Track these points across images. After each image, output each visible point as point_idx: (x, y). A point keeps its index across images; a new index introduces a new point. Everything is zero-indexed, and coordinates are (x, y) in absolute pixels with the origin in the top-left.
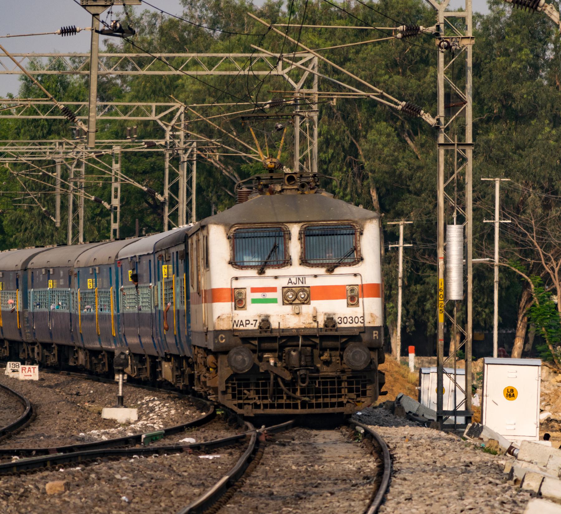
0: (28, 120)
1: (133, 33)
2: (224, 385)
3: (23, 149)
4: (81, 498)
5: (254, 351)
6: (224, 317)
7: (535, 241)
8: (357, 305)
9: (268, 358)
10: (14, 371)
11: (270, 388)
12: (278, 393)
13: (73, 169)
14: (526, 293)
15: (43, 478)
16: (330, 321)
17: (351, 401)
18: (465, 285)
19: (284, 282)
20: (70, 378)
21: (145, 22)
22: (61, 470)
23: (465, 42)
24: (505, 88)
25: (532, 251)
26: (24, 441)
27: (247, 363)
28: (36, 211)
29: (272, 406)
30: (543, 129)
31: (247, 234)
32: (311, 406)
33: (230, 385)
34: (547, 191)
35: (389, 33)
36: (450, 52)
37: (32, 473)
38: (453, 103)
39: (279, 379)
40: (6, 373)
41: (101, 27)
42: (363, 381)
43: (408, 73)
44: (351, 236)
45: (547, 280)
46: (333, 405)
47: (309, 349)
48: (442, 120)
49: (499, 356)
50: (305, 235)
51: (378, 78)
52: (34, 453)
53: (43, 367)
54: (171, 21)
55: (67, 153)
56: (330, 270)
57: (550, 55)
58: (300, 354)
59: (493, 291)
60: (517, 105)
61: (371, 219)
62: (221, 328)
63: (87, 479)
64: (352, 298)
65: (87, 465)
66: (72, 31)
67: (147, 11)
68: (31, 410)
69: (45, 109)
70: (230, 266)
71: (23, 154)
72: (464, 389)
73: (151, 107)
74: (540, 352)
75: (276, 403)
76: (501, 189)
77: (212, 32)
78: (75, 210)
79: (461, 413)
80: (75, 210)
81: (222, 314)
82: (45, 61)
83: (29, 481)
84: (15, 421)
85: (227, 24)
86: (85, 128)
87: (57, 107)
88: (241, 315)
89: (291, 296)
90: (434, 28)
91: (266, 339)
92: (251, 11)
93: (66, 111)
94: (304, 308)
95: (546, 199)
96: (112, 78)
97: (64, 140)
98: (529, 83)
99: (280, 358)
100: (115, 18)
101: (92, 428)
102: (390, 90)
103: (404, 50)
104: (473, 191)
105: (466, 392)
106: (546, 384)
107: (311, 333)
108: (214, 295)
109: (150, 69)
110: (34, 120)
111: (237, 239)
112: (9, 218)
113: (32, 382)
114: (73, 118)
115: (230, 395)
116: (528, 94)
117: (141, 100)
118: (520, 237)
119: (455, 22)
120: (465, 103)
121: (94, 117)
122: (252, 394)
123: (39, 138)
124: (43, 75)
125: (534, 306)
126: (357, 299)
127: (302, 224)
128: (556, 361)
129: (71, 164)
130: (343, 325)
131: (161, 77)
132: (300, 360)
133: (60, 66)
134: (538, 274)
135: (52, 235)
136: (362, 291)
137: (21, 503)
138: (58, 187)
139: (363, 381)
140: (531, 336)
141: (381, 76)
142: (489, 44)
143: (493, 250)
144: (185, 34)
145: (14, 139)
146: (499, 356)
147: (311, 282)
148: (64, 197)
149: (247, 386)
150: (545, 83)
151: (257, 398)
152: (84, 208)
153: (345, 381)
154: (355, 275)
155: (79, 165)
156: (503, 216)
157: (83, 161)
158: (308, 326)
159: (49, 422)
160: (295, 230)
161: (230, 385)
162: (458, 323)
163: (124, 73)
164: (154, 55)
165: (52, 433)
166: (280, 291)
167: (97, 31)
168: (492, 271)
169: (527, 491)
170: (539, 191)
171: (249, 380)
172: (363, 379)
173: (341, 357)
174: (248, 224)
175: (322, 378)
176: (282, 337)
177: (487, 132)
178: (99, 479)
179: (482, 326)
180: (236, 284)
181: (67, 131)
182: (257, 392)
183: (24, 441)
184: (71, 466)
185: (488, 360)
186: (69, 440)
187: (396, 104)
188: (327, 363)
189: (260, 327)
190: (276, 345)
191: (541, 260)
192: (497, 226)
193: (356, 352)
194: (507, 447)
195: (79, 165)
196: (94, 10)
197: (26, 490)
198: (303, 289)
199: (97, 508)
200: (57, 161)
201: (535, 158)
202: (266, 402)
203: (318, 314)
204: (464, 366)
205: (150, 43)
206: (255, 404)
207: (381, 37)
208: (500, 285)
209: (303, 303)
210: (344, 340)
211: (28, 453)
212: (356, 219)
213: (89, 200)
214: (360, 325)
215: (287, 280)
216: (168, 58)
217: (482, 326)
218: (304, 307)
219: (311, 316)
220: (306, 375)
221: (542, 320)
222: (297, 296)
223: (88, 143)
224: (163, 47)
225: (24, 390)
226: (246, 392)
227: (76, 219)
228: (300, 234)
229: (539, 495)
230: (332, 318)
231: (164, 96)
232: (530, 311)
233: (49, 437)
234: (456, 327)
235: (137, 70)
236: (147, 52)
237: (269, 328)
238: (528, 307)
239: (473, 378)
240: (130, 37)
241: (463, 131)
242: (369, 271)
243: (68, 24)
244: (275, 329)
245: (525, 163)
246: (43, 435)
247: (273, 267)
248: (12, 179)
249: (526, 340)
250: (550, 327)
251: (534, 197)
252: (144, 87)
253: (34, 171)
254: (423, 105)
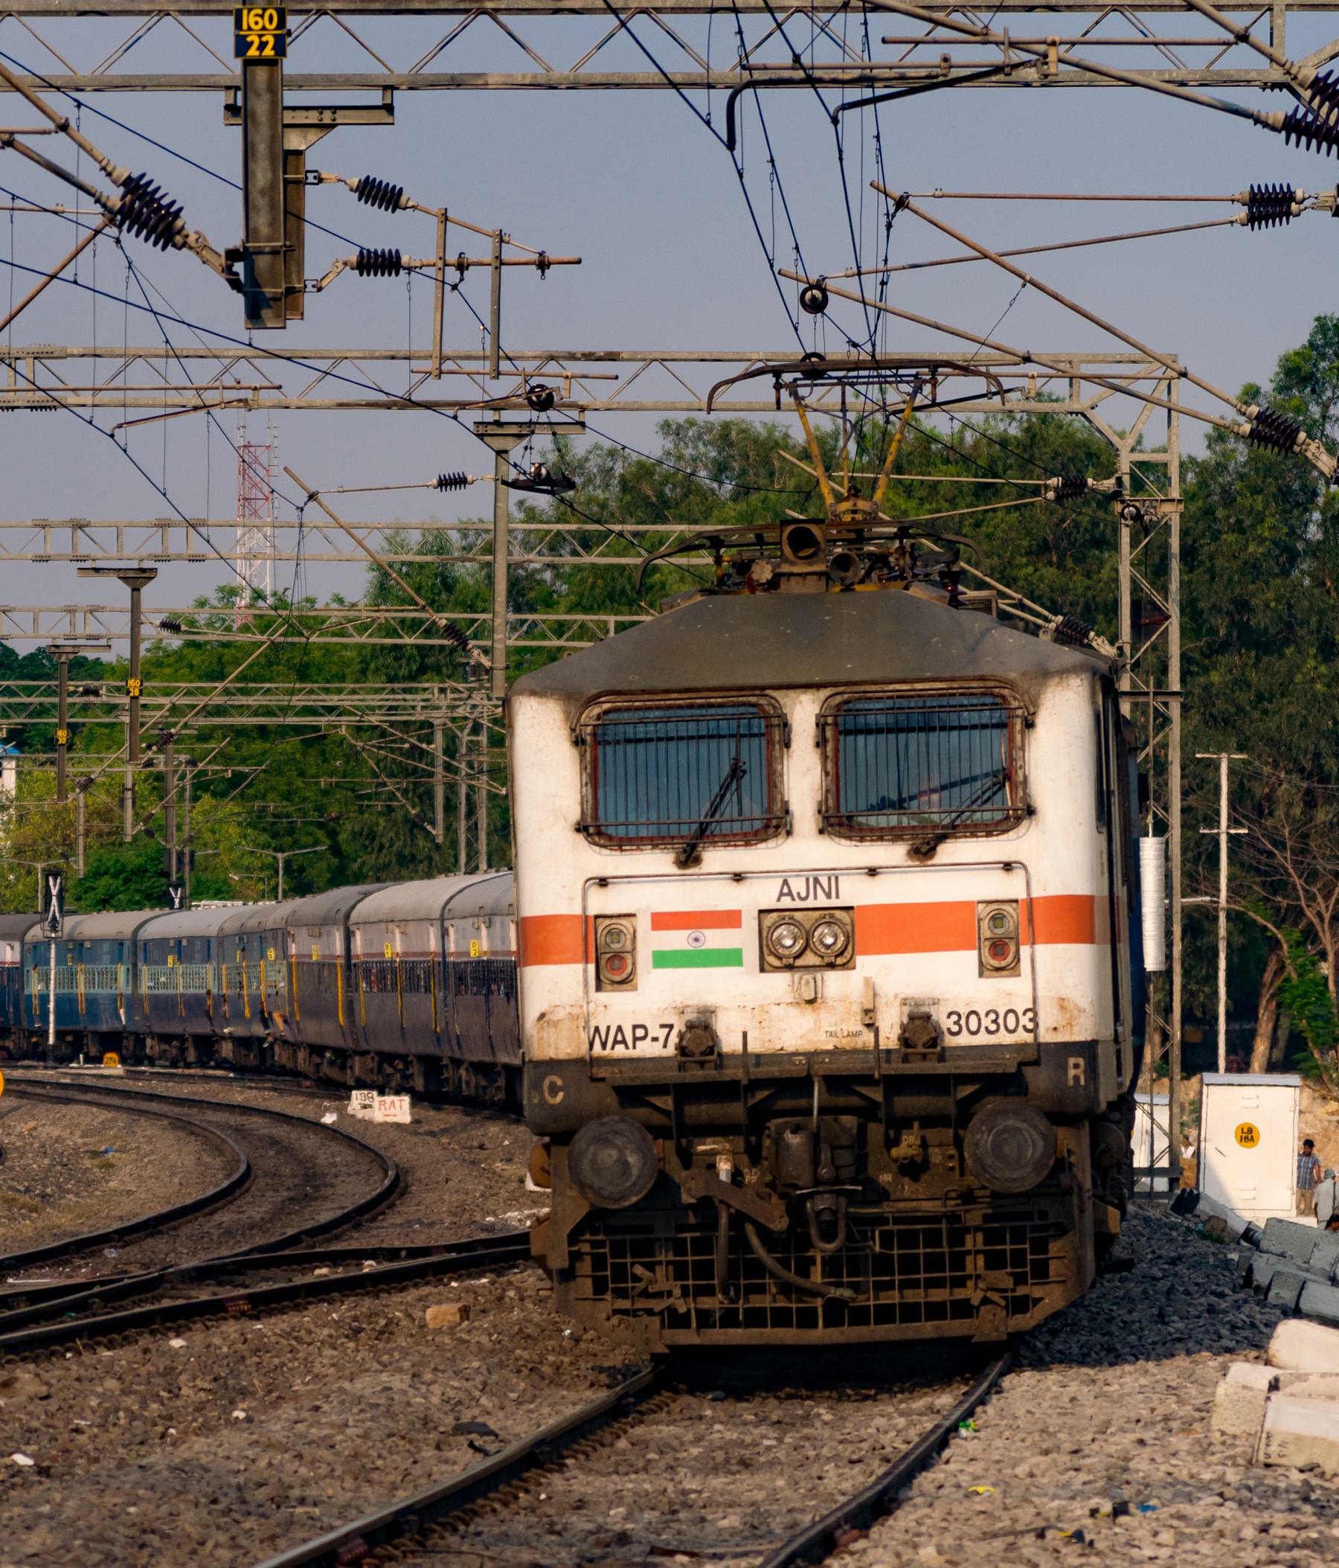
0: (383, 647)
1: (571, 485)
2: (564, 1248)
3: (373, 700)
4: (490, 1335)
5: (658, 1132)
6: (560, 1014)
7: (1289, 866)
8: (1012, 969)
9: (713, 1153)
10: (365, 1107)
11: (719, 1257)
12: (745, 1271)
13: (465, 737)
14: (1274, 959)
15: (420, 1299)
16: (921, 1029)
17: (995, 1297)
18: (1169, 945)
19: (764, 894)
20: (468, 1119)
21: (592, 466)
22: (454, 1284)
23: (1167, 508)
24: (1237, 591)
25: (1286, 883)
26: (387, 1233)
27: (635, 1172)
28: (399, 815)
29: (729, 1319)
30: (1304, 662)
31: (641, 728)
32: (860, 1317)
33: (586, 1248)
34: (1310, 776)
35: (1036, 491)
36: (1141, 526)
37: (401, 1290)
38: (1147, 618)
39: (749, 1229)
40: (350, 1110)
41: (512, 475)
42: (1034, 1229)
43: (1069, 563)
44: (996, 732)
45: (1310, 935)
46: (936, 1311)
47: (850, 1121)
48: (1127, 649)
49: (1228, 1070)
50: (838, 730)
51: (1015, 573)
52: (403, 1253)
53: (417, 1099)
54: (641, 465)
55: (454, 708)
56: (923, 851)
57: (1314, 533)
58: (816, 1139)
59: (1216, 955)
60: (1259, 620)
61: (1063, 672)
62: (551, 1053)
63: (500, 1298)
64: (998, 947)
65: (500, 1273)
66: (459, 481)
67: (598, 447)
68: (397, 1177)
69: (414, 626)
70: (580, 838)
71: (372, 709)
72: (1166, 1128)
73: (605, 623)
74: (1298, 1062)
75: (741, 1305)
76: (1231, 772)
77: (715, 485)
78: (471, 812)
79: (1162, 1172)
80: (471, 812)
82: (415, 538)
83: (395, 1304)
84: (369, 1197)
85: (743, 472)
86: (486, 662)
87: (434, 623)
88: (618, 1009)
89: (788, 942)
90: (1112, 481)
91: (703, 1088)
92: (785, 448)
93: (451, 630)
94: (834, 982)
95: (1309, 792)
96: (536, 571)
97: (450, 684)
98: (1278, 581)
99: (754, 1155)
100: (538, 460)
101: (509, 1208)
102: (1037, 593)
103: (1063, 521)
104: (1183, 777)
105: (1170, 1135)
106: (1308, 1117)
107: (856, 1067)
109: (602, 555)
110: (396, 647)
112: (349, 827)
113: (398, 1126)
114: (463, 642)
115: (589, 1282)
116: (1278, 600)
117: (587, 610)
118: (1264, 859)
119: (1148, 472)
120: (1168, 617)
121: (504, 640)
122: (662, 1279)
123: (405, 679)
124: (411, 564)
125: (1287, 980)
126: (1013, 949)
127: (827, 692)
128: (1325, 1078)
129: (462, 729)
130: (964, 1040)
131: (622, 568)
132: (816, 1162)
133: (441, 547)
134: (1296, 924)
135: (430, 859)
136: (1031, 921)
137: (381, 1345)
138: (439, 770)
139: (1034, 1229)
140: (1283, 1035)
141: (1020, 567)
142: (1209, 512)
143: (1218, 882)
144: (667, 491)
145: (357, 681)
146: (1228, 1070)
147: (856, 892)
148: (451, 788)
149: (644, 1250)
150: (1307, 582)
151: (677, 1292)
152: (488, 809)
153: (977, 1229)
154: (1008, 867)
155: (476, 729)
156: (1234, 822)
157: (485, 722)
158: (846, 1044)
159: (430, 1197)
160: (803, 712)
161: (586, 1248)
162: (1157, 1011)
163: (557, 560)
164: (612, 527)
165: (435, 1218)
166: (750, 923)
167: (504, 483)
168: (1216, 918)
169: (1275, 1306)
170: (1295, 778)
171: (650, 1229)
172: (1037, 1222)
173: (958, 1142)
174: (643, 692)
175: (897, 1221)
176: (756, 1084)
177: (1206, 670)
178: (522, 1299)
179: (1198, 1017)
180: (601, 902)
181: (455, 667)
182: (680, 1272)
183: (387, 1233)
184: (471, 1277)
185: (1208, 1077)
186: (467, 1231)
187: (1047, 620)
188: (913, 1169)
189: (682, 1049)
190: (736, 1111)
191: (1298, 899)
192: (1223, 839)
193: (1006, 1130)
194: (1241, 1229)
195: (476, 729)
196: (499, 443)
197: (390, 1321)
198: (828, 915)
199: (518, 1352)
200: (436, 722)
201: (1289, 717)
202: (706, 1303)
203: (881, 1001)
204: (1167, 1090)
205: (603, 506)
206: (672, 1310)
207: (1022, 497)
208: (1229, 946)
209: (832, 966)
210: (968, 1090)
211: (392, 1254)
212: (1013, 676)
213: (496, 795)
214: (1022, 1037)
215: (776, 885)
216: (636, 534)
217: (1198, 1017)
218: (831, 976)
219: (856, 1009)
220: (835, 1213)
221: (1303, 1006)
222: (808, 941)
223: (491, 688)
224: (627, 513)
225: (384, 1143)
226: (639, 1270)
227: (473, 829)
228: (821, 726)
229: (1297, 1313)
230: (927, 1017)
231: (630, 604)
232: (1281, 989)
233: (432, 1224)
234: (1154, 1019)
235: (578, 555)
236: (598, 522)
237: (711, 1050)
238: (1278, 983)
239: (1182, 1110)
240: (570, 494)
241: (1164, 670)
242: (1056, 847)
243: (450, 470)
244: (732, 1056)
245: (1273, 725)
246: (419, 1221)
247: (729, 840)
248: (353, 756)
249: (1274, 1042)
250: (1315, 1017)
251: (1288, 787)
252: (592, 588)
253: (395, 741)
254: (1093, 622)
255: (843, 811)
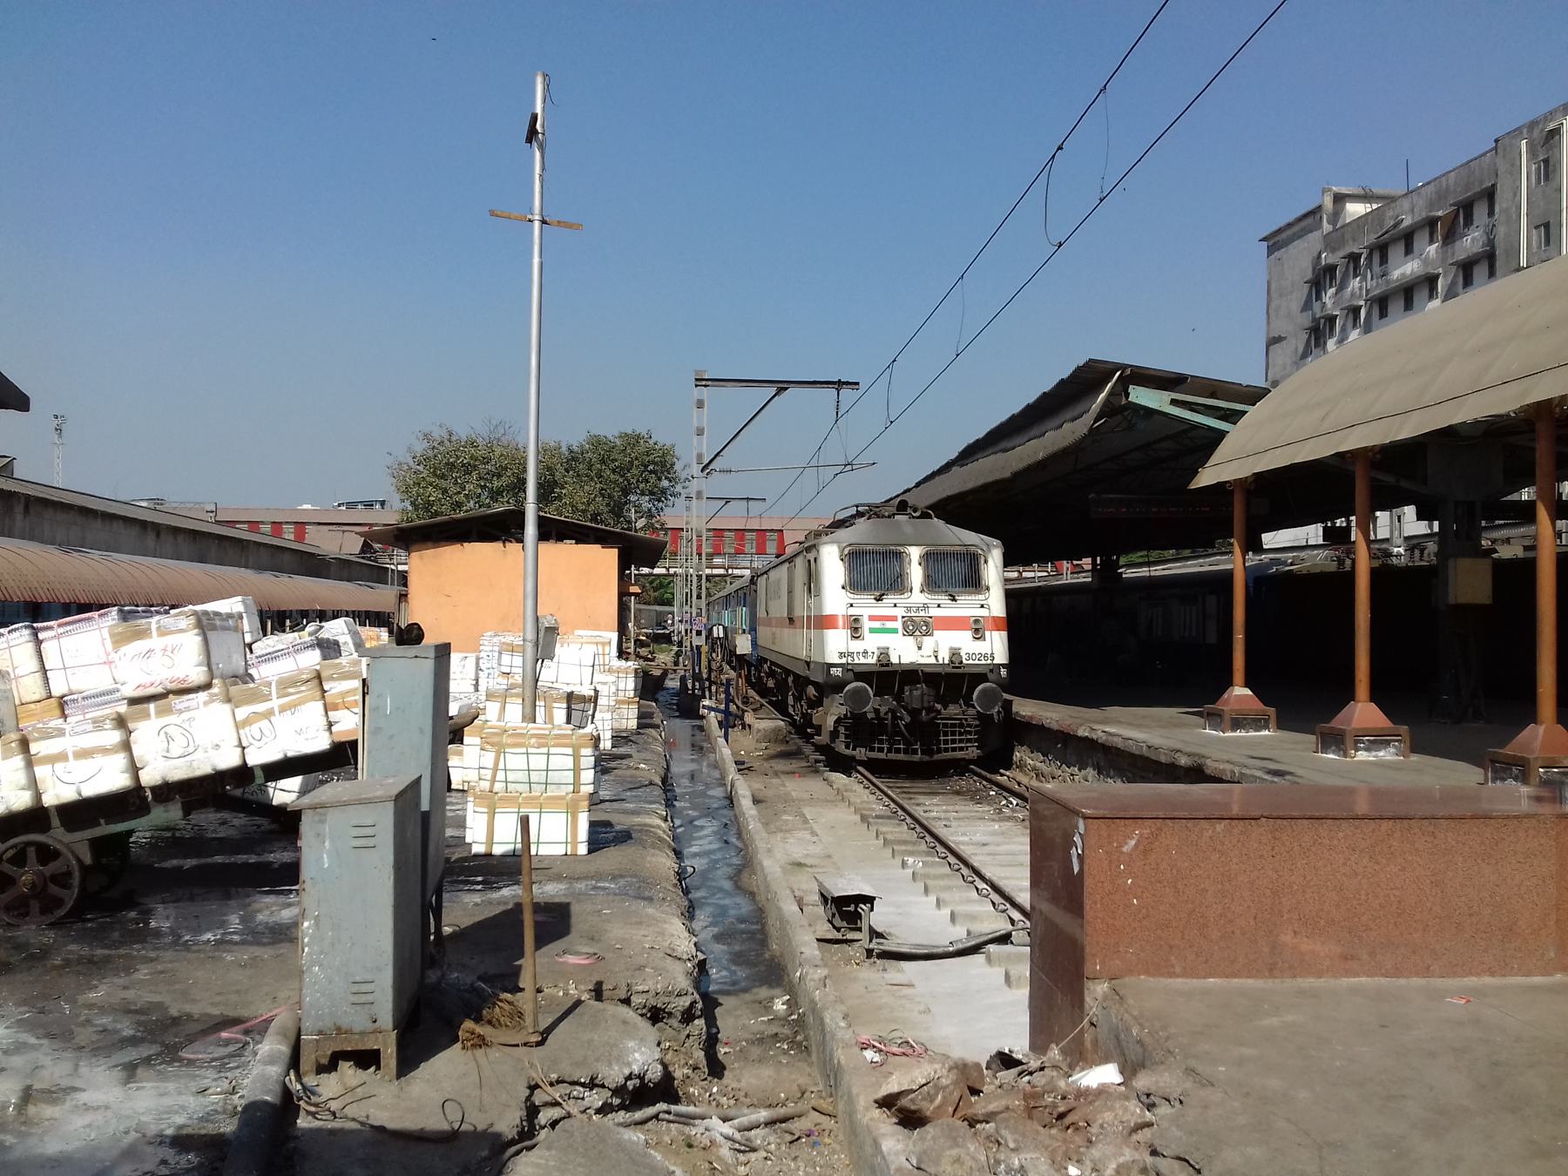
19: (900, 612)
50: (927, 558)
64: (977, 631)
81: (836, 647)
91: (887, 677)
108: (825, 622)
111: (854, 558)
147: (934, 612)
160: (915, 553)
180: (852, 611)
222: (917, 627)
255: (56, 692)
